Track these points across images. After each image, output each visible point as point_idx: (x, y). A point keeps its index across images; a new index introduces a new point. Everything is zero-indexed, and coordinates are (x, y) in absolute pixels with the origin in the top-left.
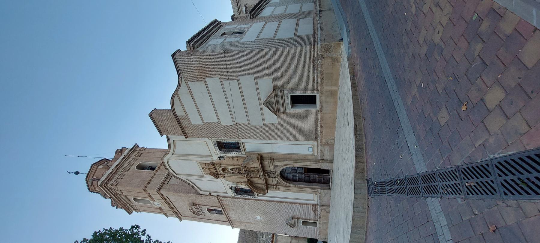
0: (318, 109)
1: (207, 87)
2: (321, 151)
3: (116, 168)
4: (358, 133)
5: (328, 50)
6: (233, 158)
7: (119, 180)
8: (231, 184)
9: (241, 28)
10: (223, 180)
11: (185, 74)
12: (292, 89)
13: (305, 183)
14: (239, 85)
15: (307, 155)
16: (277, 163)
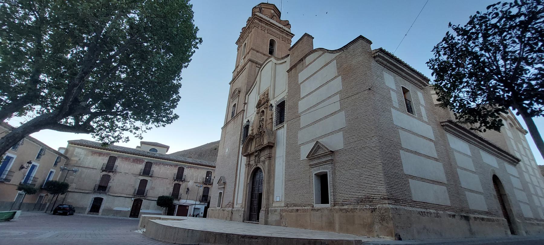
0: (315, 205)
1: (332, 79)
2: (276, 211)
3: (271, 23)
4: (247, 240)
5: (383, 219)
6: (272, 119)
7: (260, 28)
8: (252, 121)
9: (419, 110)
10: (255, 113)
11: (343, 54)
12: (334, 173)
13: (250, 194)
14: (335, 113)
15: (273, 195)
16: (267, 163)
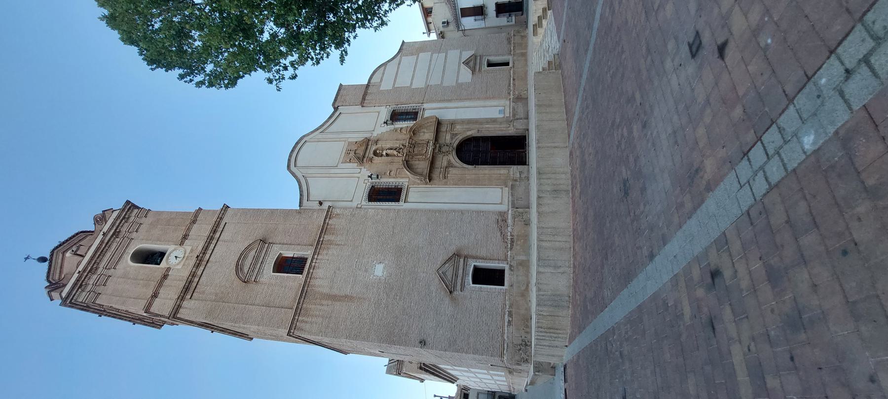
2: (514, 109)
